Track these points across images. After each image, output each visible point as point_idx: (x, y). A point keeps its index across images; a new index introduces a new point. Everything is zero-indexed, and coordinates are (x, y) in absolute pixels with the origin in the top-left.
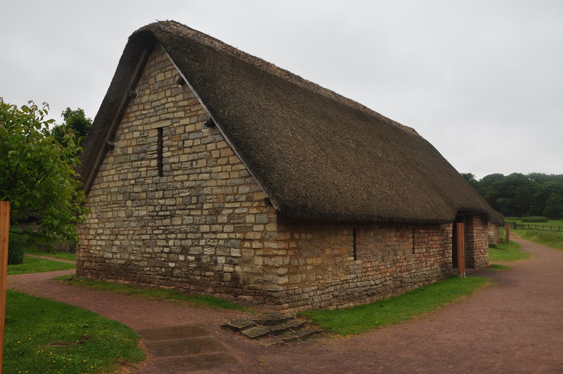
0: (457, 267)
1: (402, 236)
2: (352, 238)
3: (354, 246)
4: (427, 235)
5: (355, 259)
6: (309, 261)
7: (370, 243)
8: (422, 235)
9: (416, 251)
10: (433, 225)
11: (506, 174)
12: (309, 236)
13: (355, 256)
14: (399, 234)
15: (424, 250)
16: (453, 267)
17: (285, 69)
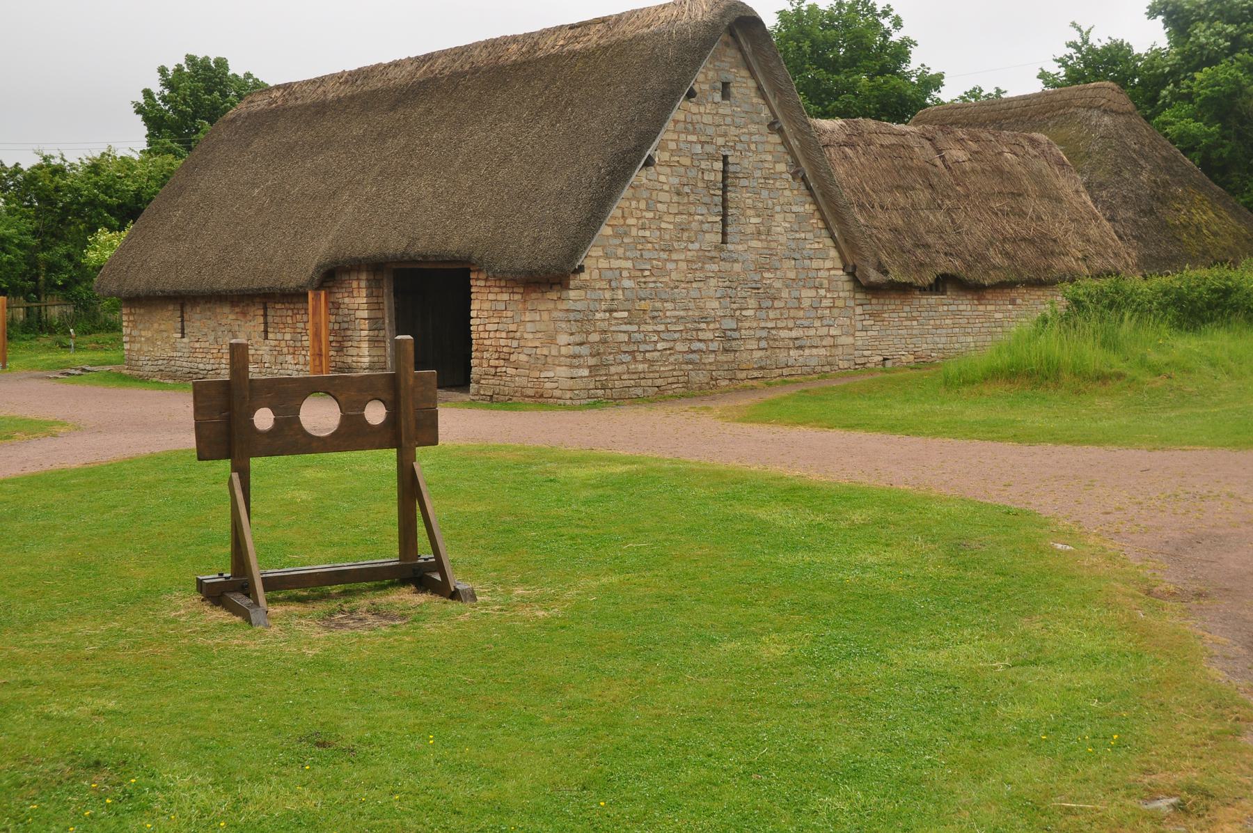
0: (233, 348)
1: (244, 314)
2: (179, 313)
3: (182, 321)
4: (290, 313)
5: (183, 337)
6: (143, 333)
7: (198, 320)
8: (279, 313)
9: (270, 336)
10: (294, 297)
11: (271, 78)
12: (142, 311)
13: (183, 333)
14: (237, 310)
15: (288, 337)
16: (245, 347)
17: (482, 38)
